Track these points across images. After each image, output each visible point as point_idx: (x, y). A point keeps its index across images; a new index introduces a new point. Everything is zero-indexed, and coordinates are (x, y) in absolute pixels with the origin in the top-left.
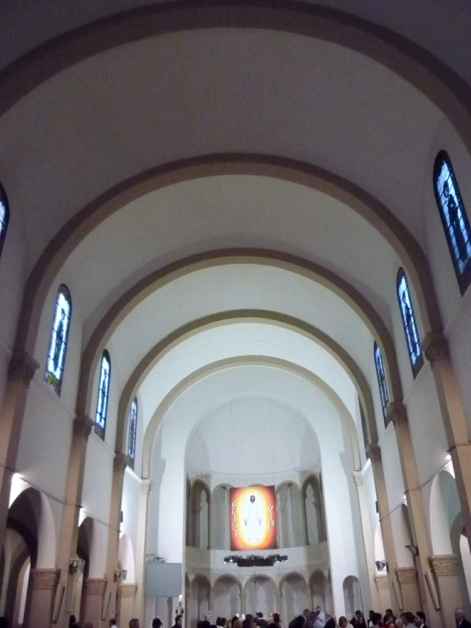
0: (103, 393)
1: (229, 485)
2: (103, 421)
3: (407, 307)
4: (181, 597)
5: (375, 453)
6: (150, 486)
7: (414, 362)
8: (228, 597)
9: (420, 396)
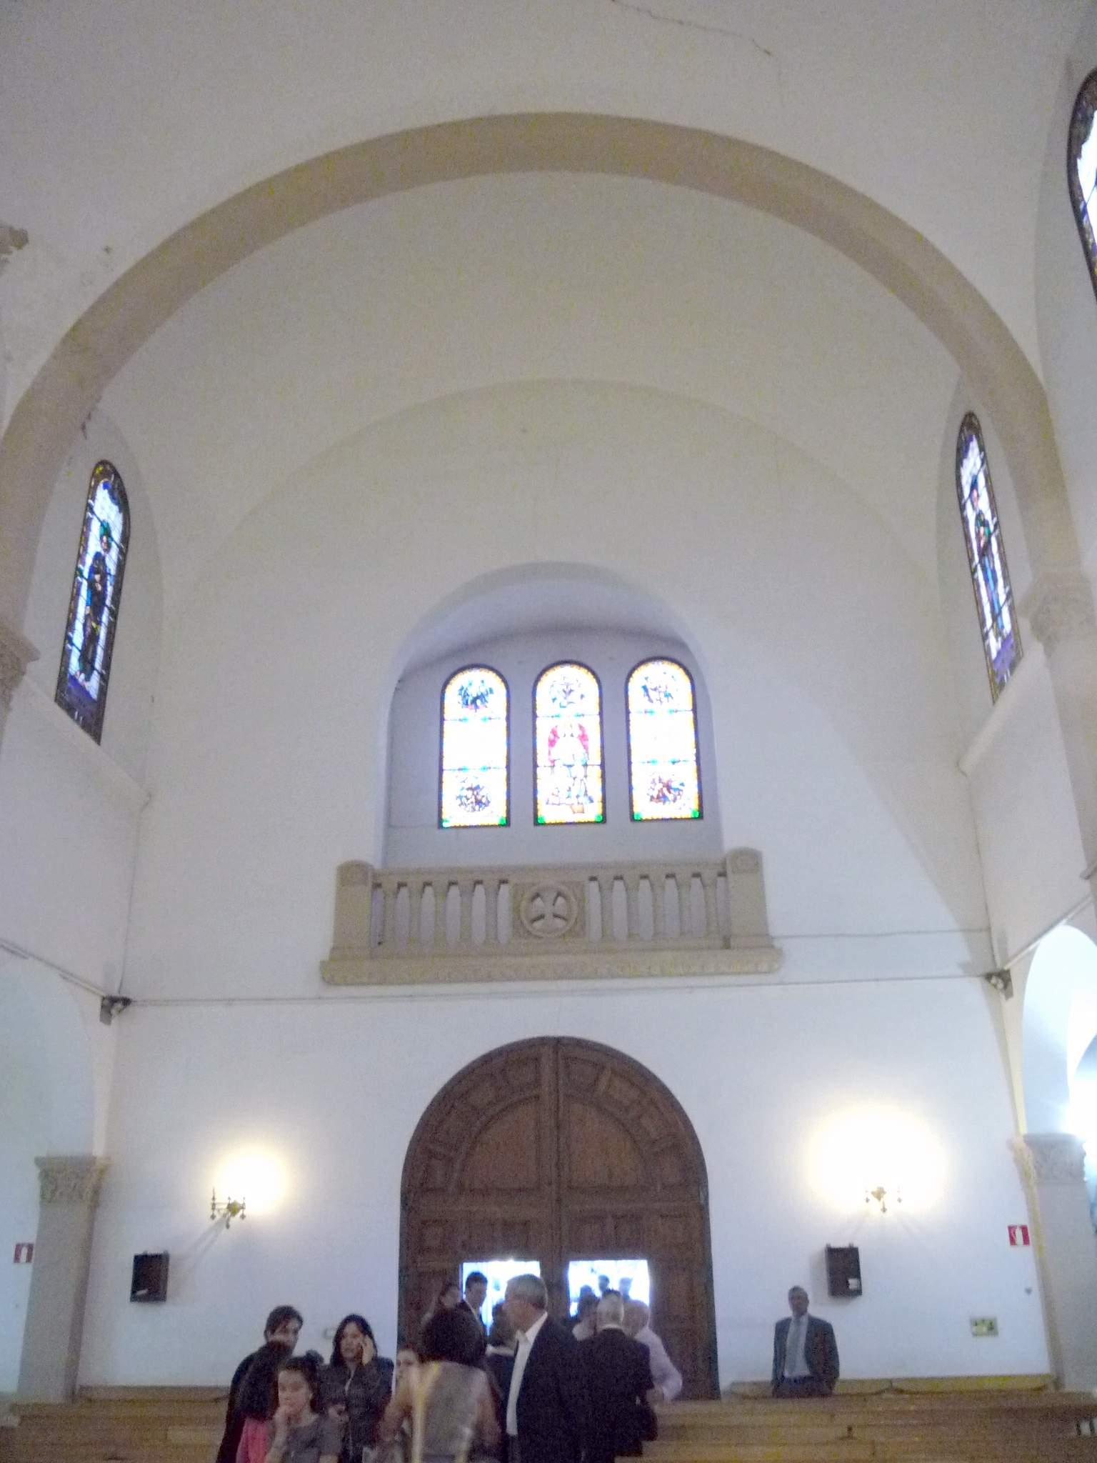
0: (97, 601)
7: (994, 655)
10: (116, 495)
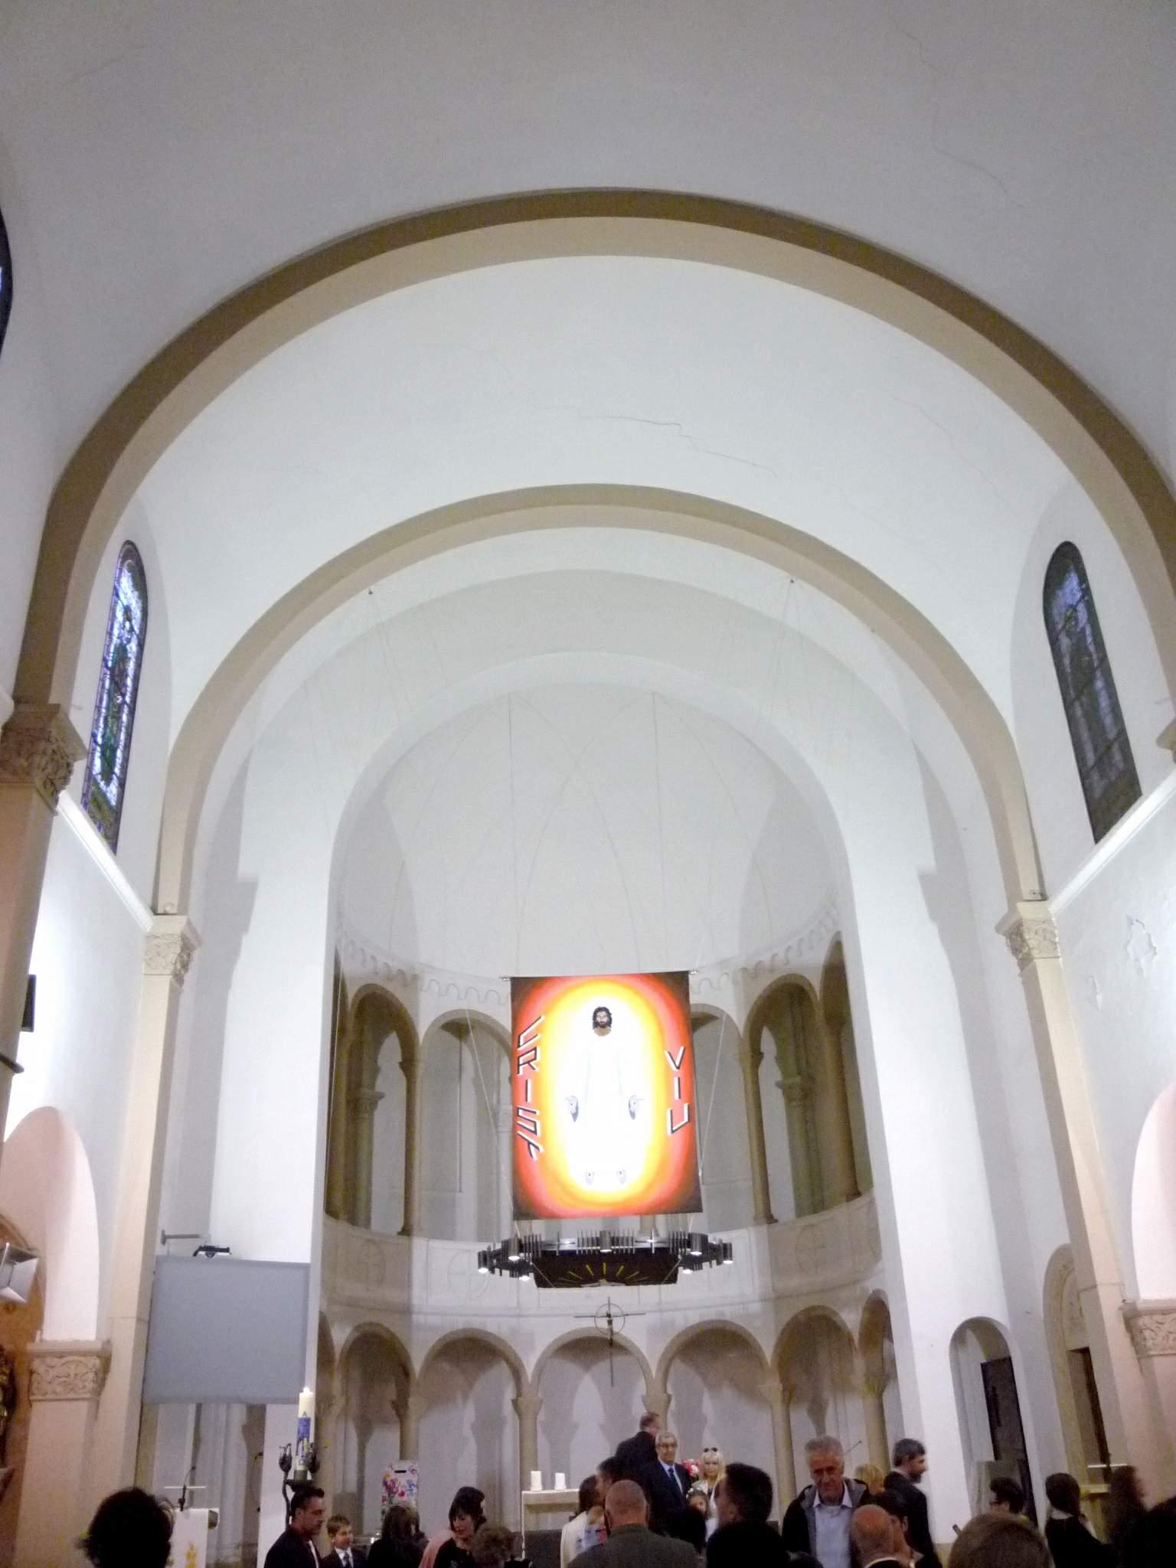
4: (307, 1396)
6: (187, 948)
8: (469, 1414)
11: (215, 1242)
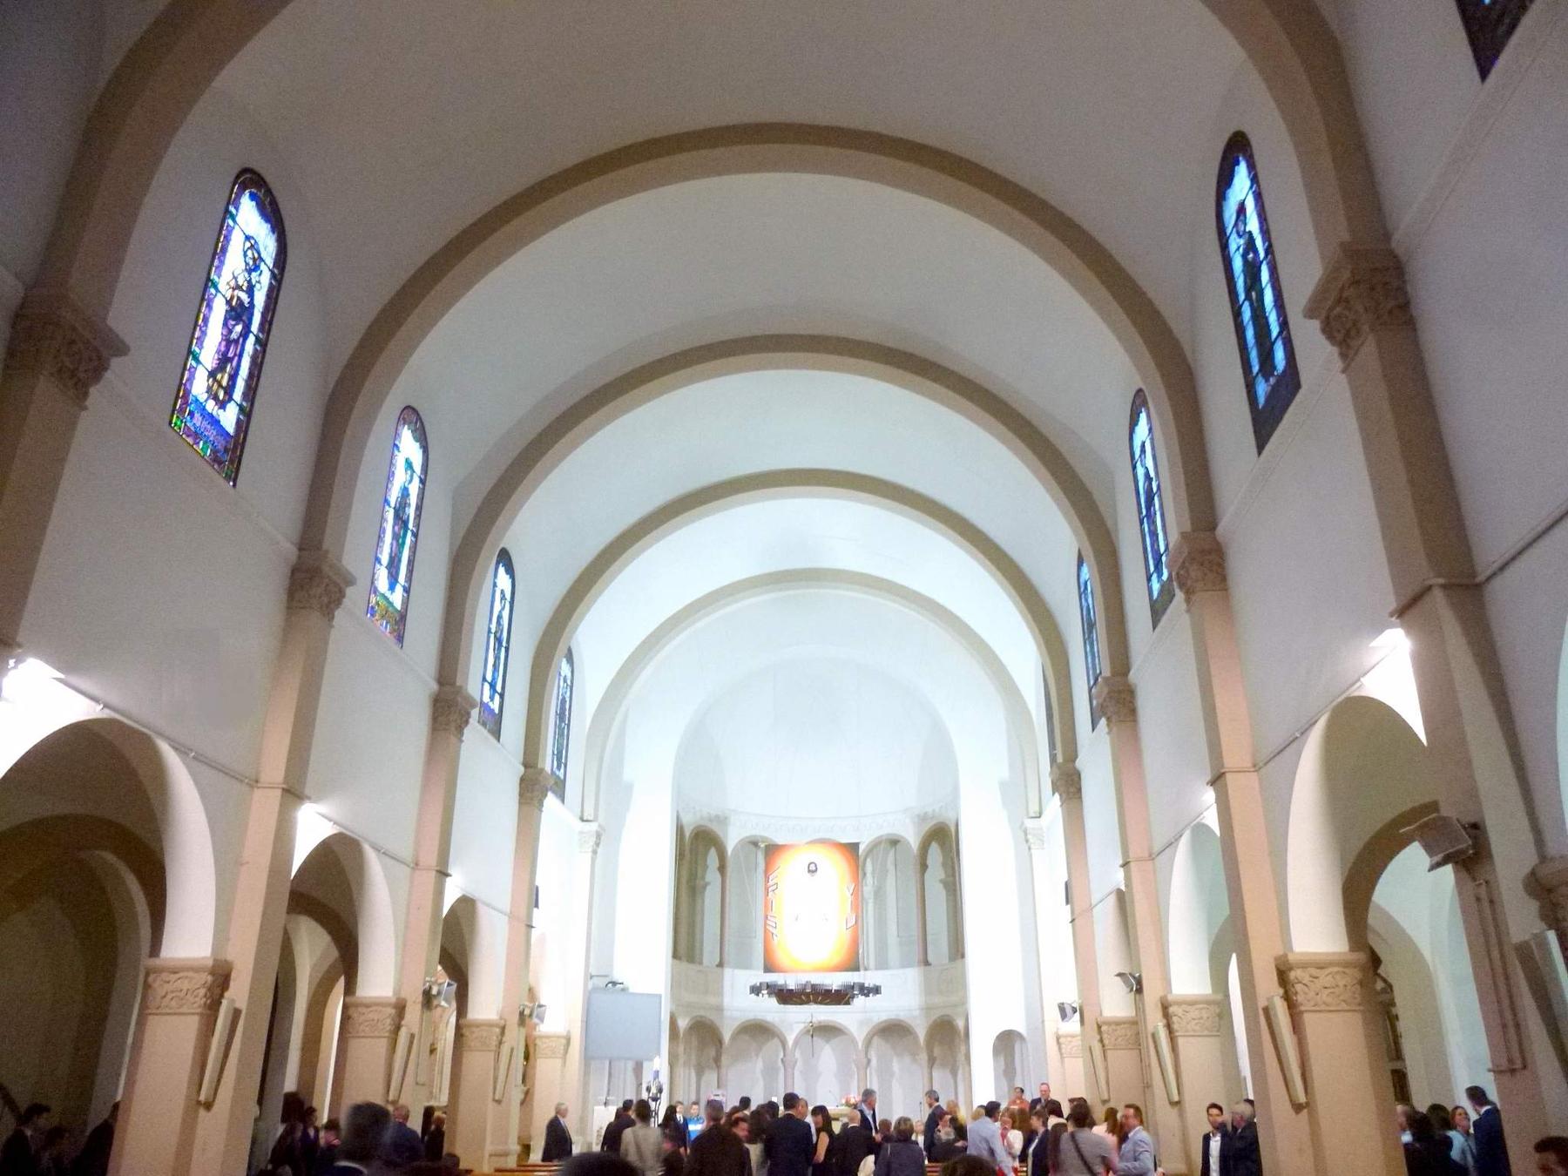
0: (498, 640)
1: (764, 839)
2: (497, 697)
3: (1147, 475)
5: (1069, 783)
6: (599, 836)
7: (1155, 594)
9: (1162, 662)
10: (269, 209)
11: (617, 977)
